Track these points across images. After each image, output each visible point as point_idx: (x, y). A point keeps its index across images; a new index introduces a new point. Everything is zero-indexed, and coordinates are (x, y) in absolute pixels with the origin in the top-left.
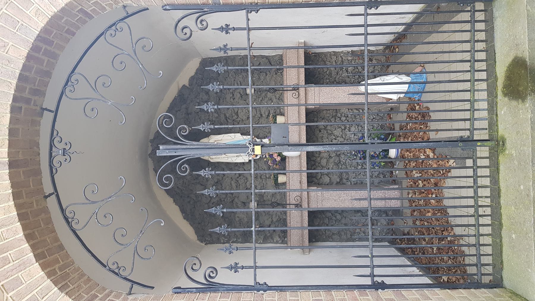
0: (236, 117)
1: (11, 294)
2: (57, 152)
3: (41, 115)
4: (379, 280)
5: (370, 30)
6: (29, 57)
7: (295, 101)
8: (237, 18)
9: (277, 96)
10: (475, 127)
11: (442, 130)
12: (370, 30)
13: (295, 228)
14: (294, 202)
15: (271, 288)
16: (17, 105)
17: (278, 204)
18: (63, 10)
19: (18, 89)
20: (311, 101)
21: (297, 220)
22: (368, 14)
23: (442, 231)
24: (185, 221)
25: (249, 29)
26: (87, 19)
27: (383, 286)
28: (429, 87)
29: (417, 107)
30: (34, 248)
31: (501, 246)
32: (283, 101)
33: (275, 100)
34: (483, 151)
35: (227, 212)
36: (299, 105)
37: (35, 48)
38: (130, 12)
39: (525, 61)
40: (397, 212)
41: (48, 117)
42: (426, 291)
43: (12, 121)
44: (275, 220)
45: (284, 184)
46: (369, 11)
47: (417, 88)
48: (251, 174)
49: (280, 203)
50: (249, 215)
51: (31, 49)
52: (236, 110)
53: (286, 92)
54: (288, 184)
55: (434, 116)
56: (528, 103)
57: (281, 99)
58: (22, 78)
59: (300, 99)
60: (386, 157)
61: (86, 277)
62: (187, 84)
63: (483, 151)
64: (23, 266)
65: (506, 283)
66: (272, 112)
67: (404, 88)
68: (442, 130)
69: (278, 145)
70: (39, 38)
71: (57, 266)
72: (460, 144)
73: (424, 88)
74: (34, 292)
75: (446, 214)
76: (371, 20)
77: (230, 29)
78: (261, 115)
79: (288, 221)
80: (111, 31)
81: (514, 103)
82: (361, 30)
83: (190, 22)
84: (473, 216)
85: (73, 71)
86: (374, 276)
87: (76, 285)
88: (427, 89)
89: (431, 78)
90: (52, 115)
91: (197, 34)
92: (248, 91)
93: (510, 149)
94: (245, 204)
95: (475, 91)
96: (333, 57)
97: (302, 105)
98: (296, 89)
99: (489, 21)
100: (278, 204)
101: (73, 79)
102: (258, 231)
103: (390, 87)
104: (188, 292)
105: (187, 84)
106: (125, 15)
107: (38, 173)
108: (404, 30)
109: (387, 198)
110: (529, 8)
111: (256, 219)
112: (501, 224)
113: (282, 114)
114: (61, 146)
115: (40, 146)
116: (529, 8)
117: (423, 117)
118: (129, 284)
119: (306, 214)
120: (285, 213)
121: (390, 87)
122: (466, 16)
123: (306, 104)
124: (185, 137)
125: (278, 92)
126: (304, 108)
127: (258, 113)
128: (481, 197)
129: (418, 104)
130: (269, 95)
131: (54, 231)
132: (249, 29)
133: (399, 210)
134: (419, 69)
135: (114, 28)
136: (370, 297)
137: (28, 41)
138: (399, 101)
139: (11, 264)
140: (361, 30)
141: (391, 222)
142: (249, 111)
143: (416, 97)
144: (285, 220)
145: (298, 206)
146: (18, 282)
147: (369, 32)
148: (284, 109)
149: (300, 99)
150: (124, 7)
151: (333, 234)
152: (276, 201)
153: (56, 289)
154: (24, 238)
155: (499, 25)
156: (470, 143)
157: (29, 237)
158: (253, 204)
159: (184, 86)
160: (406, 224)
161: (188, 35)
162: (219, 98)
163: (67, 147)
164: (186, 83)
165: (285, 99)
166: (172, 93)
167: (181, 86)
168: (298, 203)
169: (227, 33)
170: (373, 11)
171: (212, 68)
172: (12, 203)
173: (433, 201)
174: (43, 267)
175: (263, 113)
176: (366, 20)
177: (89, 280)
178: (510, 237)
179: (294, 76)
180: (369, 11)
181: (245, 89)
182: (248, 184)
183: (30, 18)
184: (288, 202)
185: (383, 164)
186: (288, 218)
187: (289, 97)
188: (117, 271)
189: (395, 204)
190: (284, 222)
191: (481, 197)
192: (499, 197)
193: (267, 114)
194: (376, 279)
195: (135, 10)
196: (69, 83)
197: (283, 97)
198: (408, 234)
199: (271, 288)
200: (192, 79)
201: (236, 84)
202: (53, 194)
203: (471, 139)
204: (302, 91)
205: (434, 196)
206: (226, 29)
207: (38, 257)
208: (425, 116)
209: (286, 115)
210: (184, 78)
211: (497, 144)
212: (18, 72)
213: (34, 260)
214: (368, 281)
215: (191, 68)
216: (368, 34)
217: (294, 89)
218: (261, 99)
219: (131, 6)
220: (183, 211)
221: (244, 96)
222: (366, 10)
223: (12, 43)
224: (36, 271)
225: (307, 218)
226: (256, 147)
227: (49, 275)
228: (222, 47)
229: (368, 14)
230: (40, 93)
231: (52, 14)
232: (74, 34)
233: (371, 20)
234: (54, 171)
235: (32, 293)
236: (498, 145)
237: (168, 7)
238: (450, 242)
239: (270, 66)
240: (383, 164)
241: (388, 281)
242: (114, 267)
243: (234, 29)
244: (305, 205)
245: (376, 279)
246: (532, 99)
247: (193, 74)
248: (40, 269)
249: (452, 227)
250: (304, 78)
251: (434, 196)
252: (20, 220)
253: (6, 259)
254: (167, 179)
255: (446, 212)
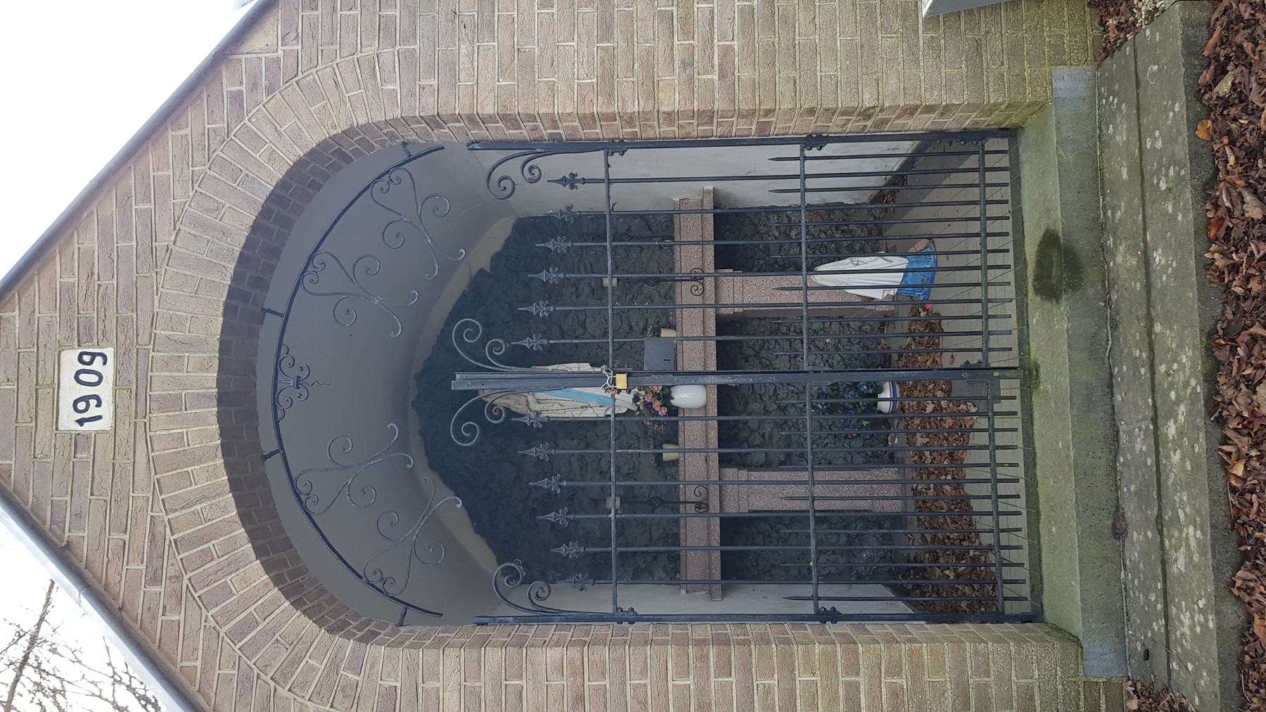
0: (581, 331)
1: (213, 612)
2: (286, 381)
3: (261, 320)
4: (828, 605)
5: (810, 183)
6: (255, 227)
7: (697, 300)
8: (590, 164)
9: (663, 291)
10: (991, 346)
11: (958, 351)
12: (810, 183)
13: (694, 548)
14: (694, 499)
15: (641, 618)
16: (233, 302)
17: (663, 503)
18: (312, 153)
19: (237, 277)
20: (726, 298)
21: (700, 535)
22: (806, 158)
23: (961, 540)
24: (478, 537)
25: (610, 182)
26: (343, 164)
27: (835, 617)
28: (940, 278)
29: (923, 314)
30: (253, 536)
31: (1040, 550)
32: (673, 300)
33: (657, 299)
34: (1009, 386)
35: (567, 487)
36: (704, 306)
37: (265, 213)
38: (413, 153)
39: (1058, 237)
40: (897, 520)
41: (273, 323)
42: (908, 625)
43: (226, 329)
44: (656, 535)
45: (675, 463)
46: (808, 153)
47: (918, 278)
48: (605, 247)
49: (670, 501)
50: (605, 524)
51: (260, 214)
52: (582, 317)
53: (678, 284)
54: (681, 463)
55: (947, 326)
56: (1063, 306)
57: (669, 297)
58: (243, 260)
59: (708, 295)
60: (874, 412)
61: (328, 595)
62: (487, 267)
63: (1009, 386)
64: (235, 564)
65: (1048, 614)
66: (651, 321)
67: (897, 278)
68: (958, 351)
69: (656, 373)
70: (274, 197)
71: (284, 570)
72: (965, 374)
73: (933, 278)
74: (251, 609)
75: (970, 512)
76: (811, 167)
77: (579, 181)
78: (631, 328)
79: (682, 537)
80: (382, 184)
81: (1048, 305)
82: (796, 184)
83: (513, 168)
84: (988, 497)
85: (316, 250)
86: (819, 599)
87: (315, 603)
88: (937, 281)
89: (943, 261)
90: (280, 320)
91: (524, 188)
92: (606, 282)
93: (1045, 385)
94: (598, 503)
95: (988, 284)
96: (771, 216)
97: (711, 306)
98: (698, 278)
99: (1015, 168)
100: (663, 503)
101: (316, 261)
102: (621, 553)
103: (869, 278)
104: (500, 622)
105: (487, 267)
106: (406, 157)
107: (253, 416)
108: (902, 168)
109: (872, 490)
110: (1061, 152)
111: (618, 535)
112: (1038, 513)
113: (672, 326)
114: (295, 372)
115: (258, 372)
116: (1061, 152)
117: (932, 330)
118: (401, 608)
119: (716, 522)
120: (677, 521)
121: (869, 278)
122: (972, 161)
123: (717, 305)
124: (501, 360)
125: (665, 283)
126: (711, 313)
127: (626, 323)
128: (1002, 465)
129: (924, 309)
130: (647, 289)
131: (276, 516)
132: (610, 182)
133: (900, 517)
134: (921, 245)
135: (386, 177)
136: (809, 631)
137: (255, 201)
138: (895, 300)
139: (214, 562)
140: (796, 184)
141: (887, 539)
142: (606, 320)
143: (920, 295)
144: (677, 536)
145: (702, 506)
146: (226, 592)
147: (808, 186)
148: (675, 317)
149: (708, 295)
150: (404, 144)
151: (774, 566)
152: (658, 500)
153: (287, 603)
154: (237, 519)
155: (1027, 172)
156: (980, 373)
157: (245, 518)
158: (613, 502)
159: (482, 271)
160: (911, 543)
161: (509, 191)
162: (551, 294)
163: (303, 375)
164: (485, 263)
165: (678, 296)
166: (458, 284)
167: (475, 271)
168: (699, 499)
169: (572, 187)
170: (814, 152)
171: (546, 245)
172: (220, 461)
173: (948, 488)
174: (268, 568)
175: (633, 324)
176: (803, 167)
177: (333, 599)
178: (1050, 531)
179: (695, 252)
180: (808, 153)
181: (601, 279)
182: (603, 462)
183: (260, 165)
184: (682, 499)
185: (865, 423)
186: (682, 531)
187: (685, 293)
188: (379, 585)
189: (895, 507)
190: (675, 539)
191: (1002, 465)
192: (1035, 465)
193: (642, 326)
194: (821, 604)
195: (424, 150)
196: (310, 268)
197: (674, 292)
198: (915, 560)
199: (641, 618)
200: (497, 257)
201: (582, 269)
202: (277, 452)
203: (983, 366)
204: (709, 283)
205: (949, 477)
206: (571, 181)
207: (260, 552)
208: (933, 327)
209: (678, 327)
210: (482, 256)
211: (1028, 374)
212: (238, 250)
213: (253, 555)
214: (809, 608)
215: (498, 235)
216: (806, 190)
217: (695, 279)
218: (630, 296)
219: (415, 143)
220: (473, 515)
221: (598, 290)
222: (802, 151)
223: (228, 205)
224: (256, 573)
225: (718, 528)
226: (618, 376)
227: (277, 581)
228: (564, 210)
229: (806, 158)
230: (262, 284)
231: (296, 159)
232: (319, 187)
233: (811, 167)
234: (280, 414)
235: (248, 611)
236: (1030, 373)
237: (476, 146)
238: (974, 559)
239: (657, 228)
240: (865, 423)
241: (843, 608)
242: (374, 579)
243: (584, 181)
244: (714, 506)
245: (821, 604)
246: (1068, 299)
247: (498, 247)
248: (262, 572)
249: (977, 533)
250: (712, 258)
251: (949, 477)
252: (232, 490)
253: (206, 553)
254: (470, 429)
255: (968, 505)
